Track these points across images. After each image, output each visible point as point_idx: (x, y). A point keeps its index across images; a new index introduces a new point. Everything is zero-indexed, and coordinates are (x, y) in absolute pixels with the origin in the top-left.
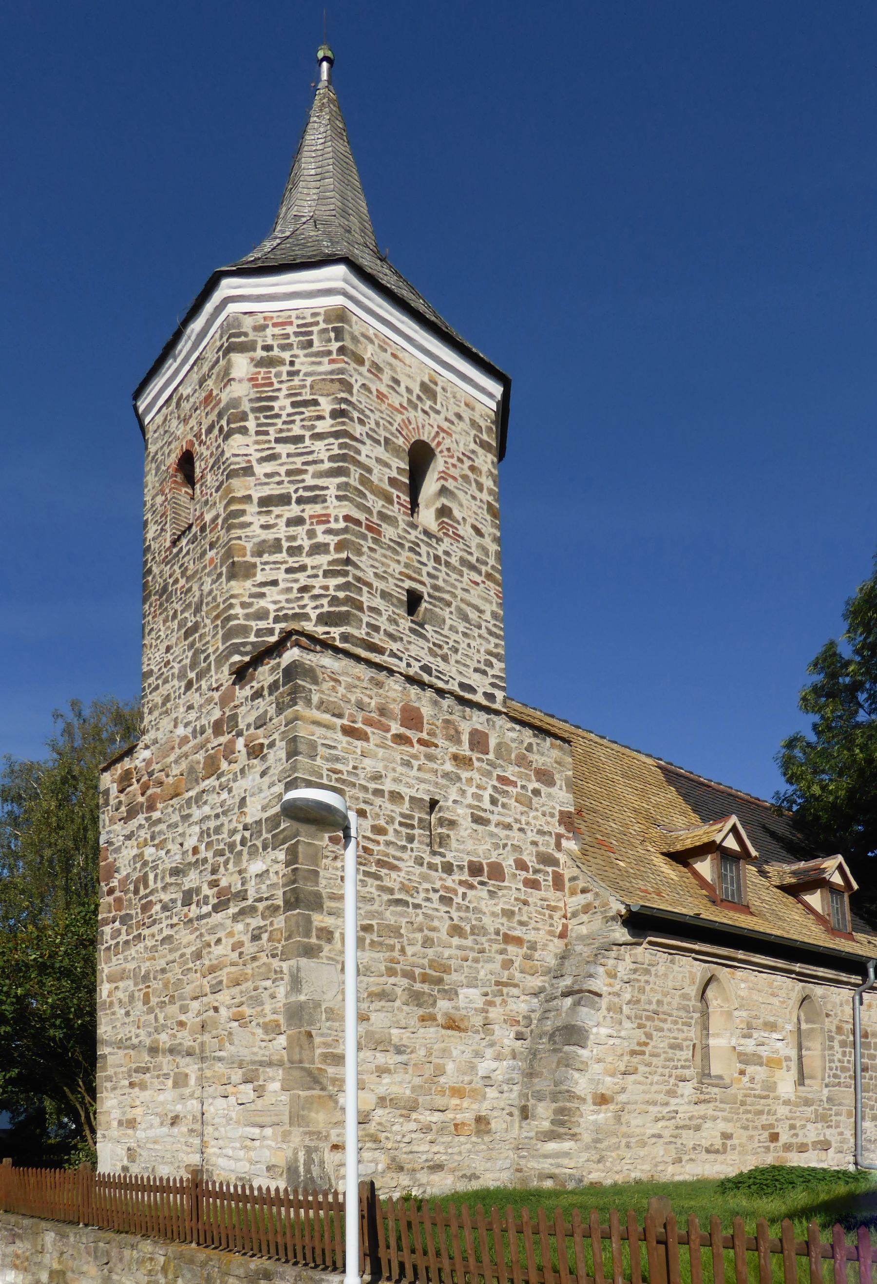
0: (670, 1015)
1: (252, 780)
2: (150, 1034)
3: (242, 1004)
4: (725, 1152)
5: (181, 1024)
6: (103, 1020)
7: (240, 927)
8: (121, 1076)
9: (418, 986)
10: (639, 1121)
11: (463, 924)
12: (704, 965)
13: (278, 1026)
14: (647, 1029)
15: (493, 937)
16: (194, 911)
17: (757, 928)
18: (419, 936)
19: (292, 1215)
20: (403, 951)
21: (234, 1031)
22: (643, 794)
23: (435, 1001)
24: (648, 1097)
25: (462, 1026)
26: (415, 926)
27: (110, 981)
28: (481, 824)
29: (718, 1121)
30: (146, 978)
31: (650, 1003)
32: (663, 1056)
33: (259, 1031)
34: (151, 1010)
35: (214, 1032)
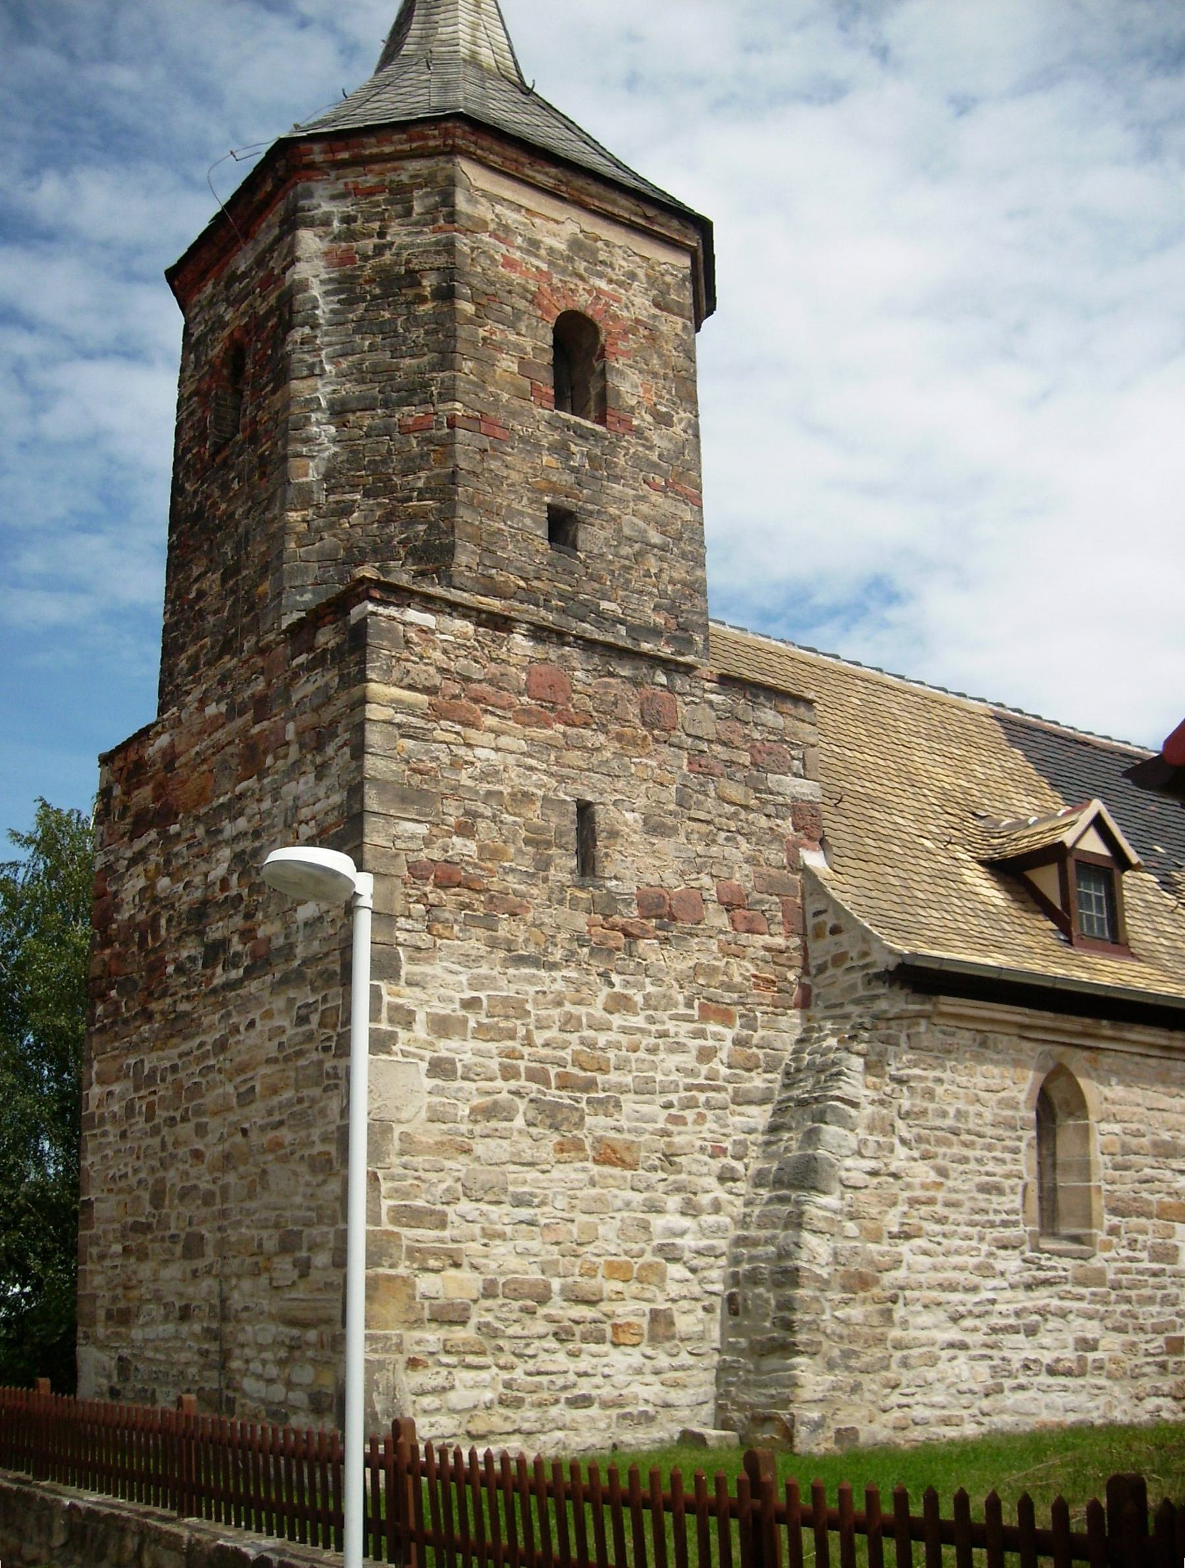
0: (980, 1135)
1: (303, 786)
2: (153, 1170)
3: (281, 1123)
4: (1082, 1374)
5: (197, 1155)
6: (90, 1145)
7: (279, 1003)
8: (111, 1237)
9: (553, 1094)
10: (926, 1319)
11: (630, 992)
12: (1047, 1047)
13: (330, 1161)
14: (939, 1161)
15: (682, 1010)
16: (220, 977)
17: (1140, 984)
18: (556, 1013)
19: (273, 1496)
20: (528, 1041)
21: (269, 1167)
22: (960, 767)
23: (582, 1118)
24: (941, 1276)
25: (628, 1159)
26: (550, 997)
27: (102, 1081)
28: (662, 834)
29: (1071, 1317)
30: (151, 1078)
31: (944, 1114)
32: (968, 1205)
33: (303, 1169)
34: (156, 1131)
35: (242, 1169)
